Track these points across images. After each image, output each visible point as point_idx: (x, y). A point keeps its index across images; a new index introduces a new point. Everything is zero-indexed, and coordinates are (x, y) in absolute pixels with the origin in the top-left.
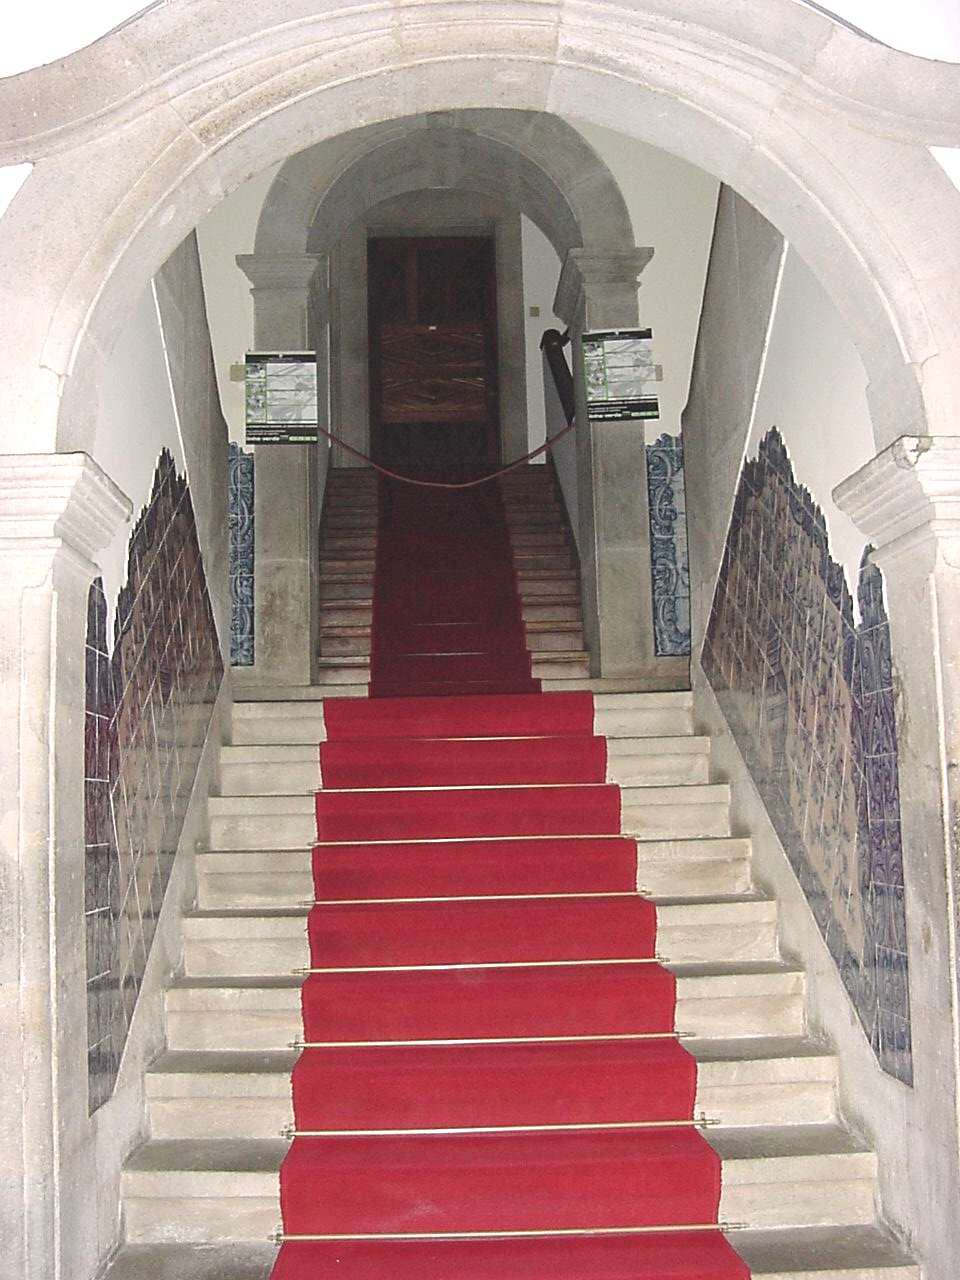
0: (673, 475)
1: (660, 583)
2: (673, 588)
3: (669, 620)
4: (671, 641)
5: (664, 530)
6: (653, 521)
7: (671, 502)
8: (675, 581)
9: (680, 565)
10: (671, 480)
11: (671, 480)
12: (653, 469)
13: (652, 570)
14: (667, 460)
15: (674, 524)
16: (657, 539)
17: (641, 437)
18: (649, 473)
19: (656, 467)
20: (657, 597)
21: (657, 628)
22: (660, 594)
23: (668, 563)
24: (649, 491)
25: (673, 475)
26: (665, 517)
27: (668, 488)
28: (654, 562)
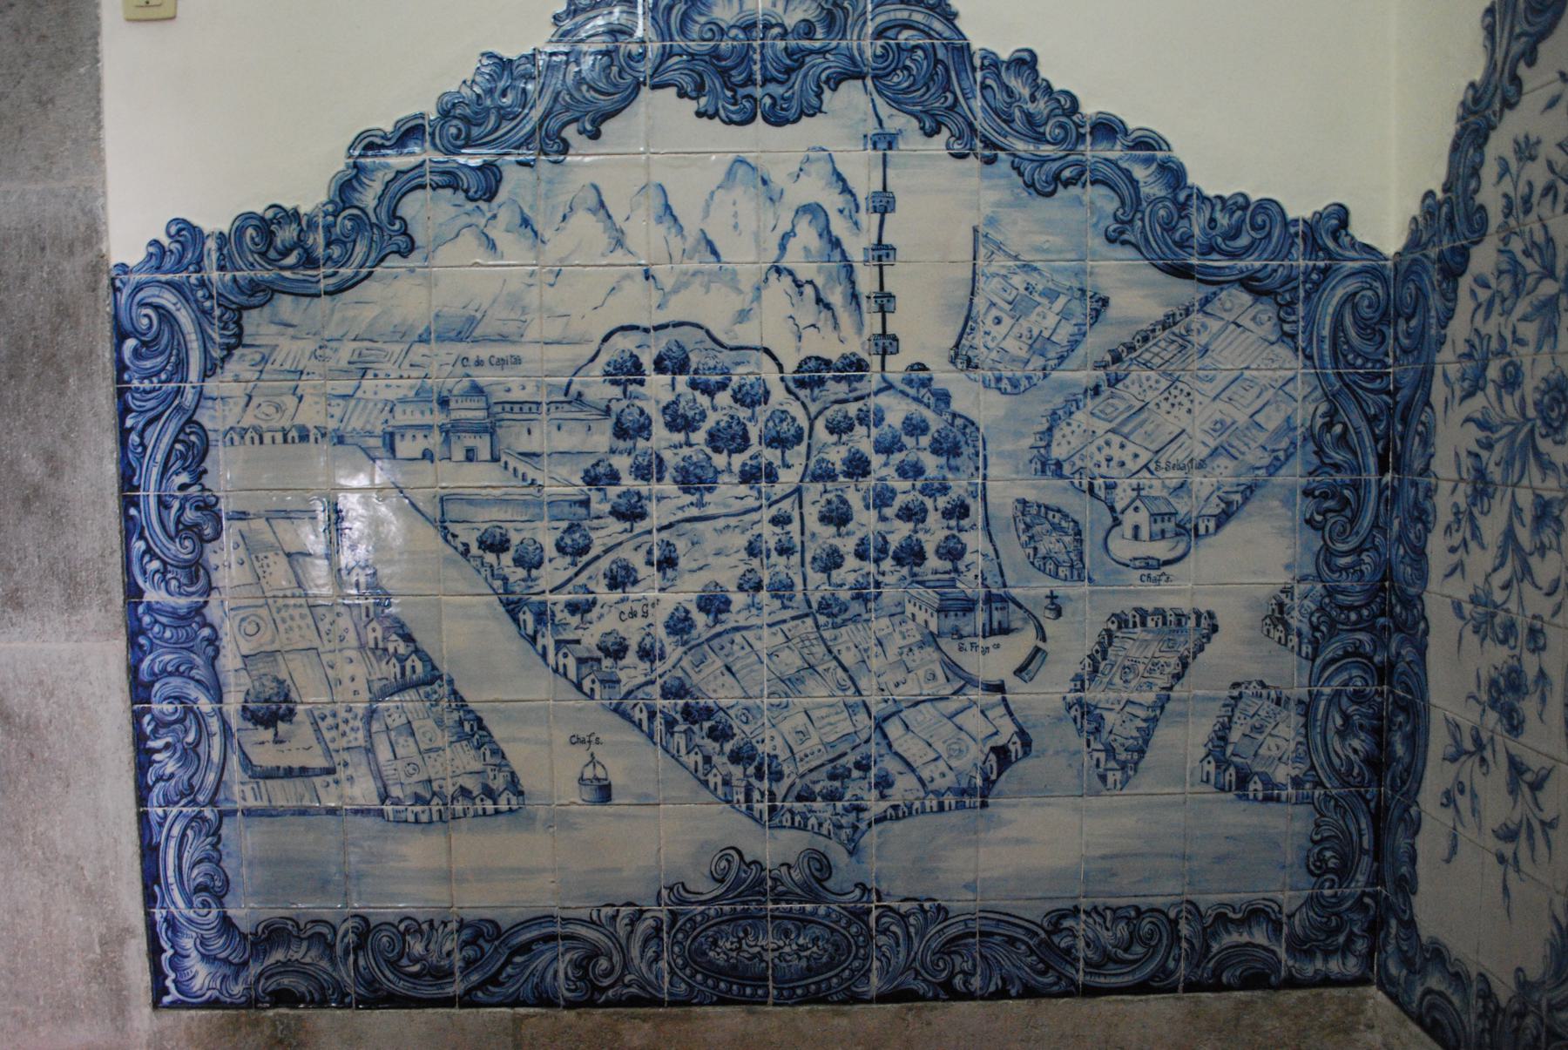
0: (208, 372)
1: (167, 763)
2: (211, 777)
3: (200, 889)
4: (205, 958)
5: (176, 578)
6: (139, 546)
7: (198, 476)
8: (216, 756)
9: (233, 703)
10: (201, 394)
11: (201, 394)
12: (136, 353)
13: (137, 717)
14: (185, 318)
15: (212, 558)
16: (150, 608)
17: (93, 233)
18: (121, 367)
19: (147, 346)
20: (156, 811)
21: (159, 914)
22: (169, 803)
23: (193, 692)
24: (124, 433)
25: (208, 372)
26: (183, 530)
27: (190, 421)
28: (140, 690)
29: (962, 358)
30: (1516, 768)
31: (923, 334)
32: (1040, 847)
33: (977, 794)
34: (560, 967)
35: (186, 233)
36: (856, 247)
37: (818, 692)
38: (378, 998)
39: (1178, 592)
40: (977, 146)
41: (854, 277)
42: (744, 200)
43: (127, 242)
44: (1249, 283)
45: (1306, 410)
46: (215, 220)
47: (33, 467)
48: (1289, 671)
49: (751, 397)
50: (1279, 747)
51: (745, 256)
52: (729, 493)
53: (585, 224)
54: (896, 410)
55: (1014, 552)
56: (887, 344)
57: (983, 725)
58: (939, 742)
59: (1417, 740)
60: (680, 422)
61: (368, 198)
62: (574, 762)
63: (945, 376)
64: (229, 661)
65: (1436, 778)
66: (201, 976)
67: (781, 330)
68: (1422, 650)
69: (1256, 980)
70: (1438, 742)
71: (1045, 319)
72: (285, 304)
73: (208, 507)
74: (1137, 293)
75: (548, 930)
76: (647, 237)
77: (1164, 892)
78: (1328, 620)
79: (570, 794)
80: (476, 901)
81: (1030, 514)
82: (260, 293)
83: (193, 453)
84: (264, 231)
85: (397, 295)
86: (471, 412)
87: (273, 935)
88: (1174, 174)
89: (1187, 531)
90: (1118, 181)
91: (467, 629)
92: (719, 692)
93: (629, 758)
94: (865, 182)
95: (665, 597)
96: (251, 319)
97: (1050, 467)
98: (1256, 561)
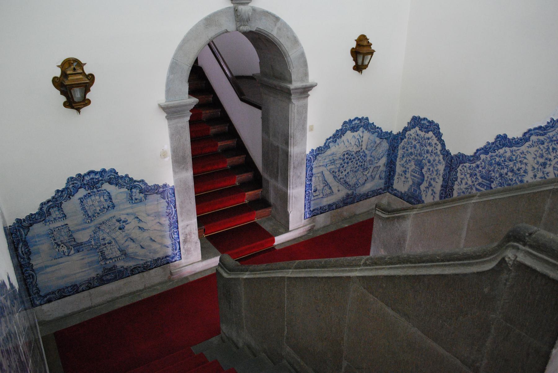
1: (307, 198)
17: (305, 152)
29: (366, 149)
30: (405, 177)
31: (364, 147)
32: (368, 187)
33: (364, 184)
34: (334, 207)
35: (313, 150)
36: (360, 141)
37: (354, 178)
38: (321, 213)
39: (378, 165)
40: (369, 131)
41: (360, 144)
42: (353, 139)
43: (308, 152)
44: (385, 138)
45: (388, 148)
46: (315, 149)
47: (299, 174)
48: (384, 169)
49: (352, 155)
50: (383, 175)
51: (353, 144)
52: (350, 163)
53: (342, 143)
54: (362, 154)
55: (368, 164)
56: (362, 149)
57: (365, 178)
58: (361, 181)
59: (394, 174)
60: (347, 158)
61: (327, 144)
62: (337, 189)
63: (365, 151)
64: (313, 187)
65: (396, 177)
66: (308, 216)
67: (355, 149)
68: (395, 167)
69: (380, 194)
70: (397, 174)
71: (372, 145)
72: (320, 155)
73: (312, 174)
74: (378, 141)
75: (334, 203)
76: (346, 143)
77: (375, 188)
78: (387, 164)
79: (337, 191)
80: (329, 203)
81: (370, 160)
82: (318, 154)
83: (311, 170)
84: (319, 149)
85: (329, 152)
86: (332, 161)
87: (314, 210)
88: (381, 130)
89: (379, 159)
90: (378, 132)
91: (330, 179)
92: (348, 180)
93: (341, 187)
94: (361, 136)
95: (344, 173)
96: (317, 157)
97: (371, 156)
98: (384, 160)
